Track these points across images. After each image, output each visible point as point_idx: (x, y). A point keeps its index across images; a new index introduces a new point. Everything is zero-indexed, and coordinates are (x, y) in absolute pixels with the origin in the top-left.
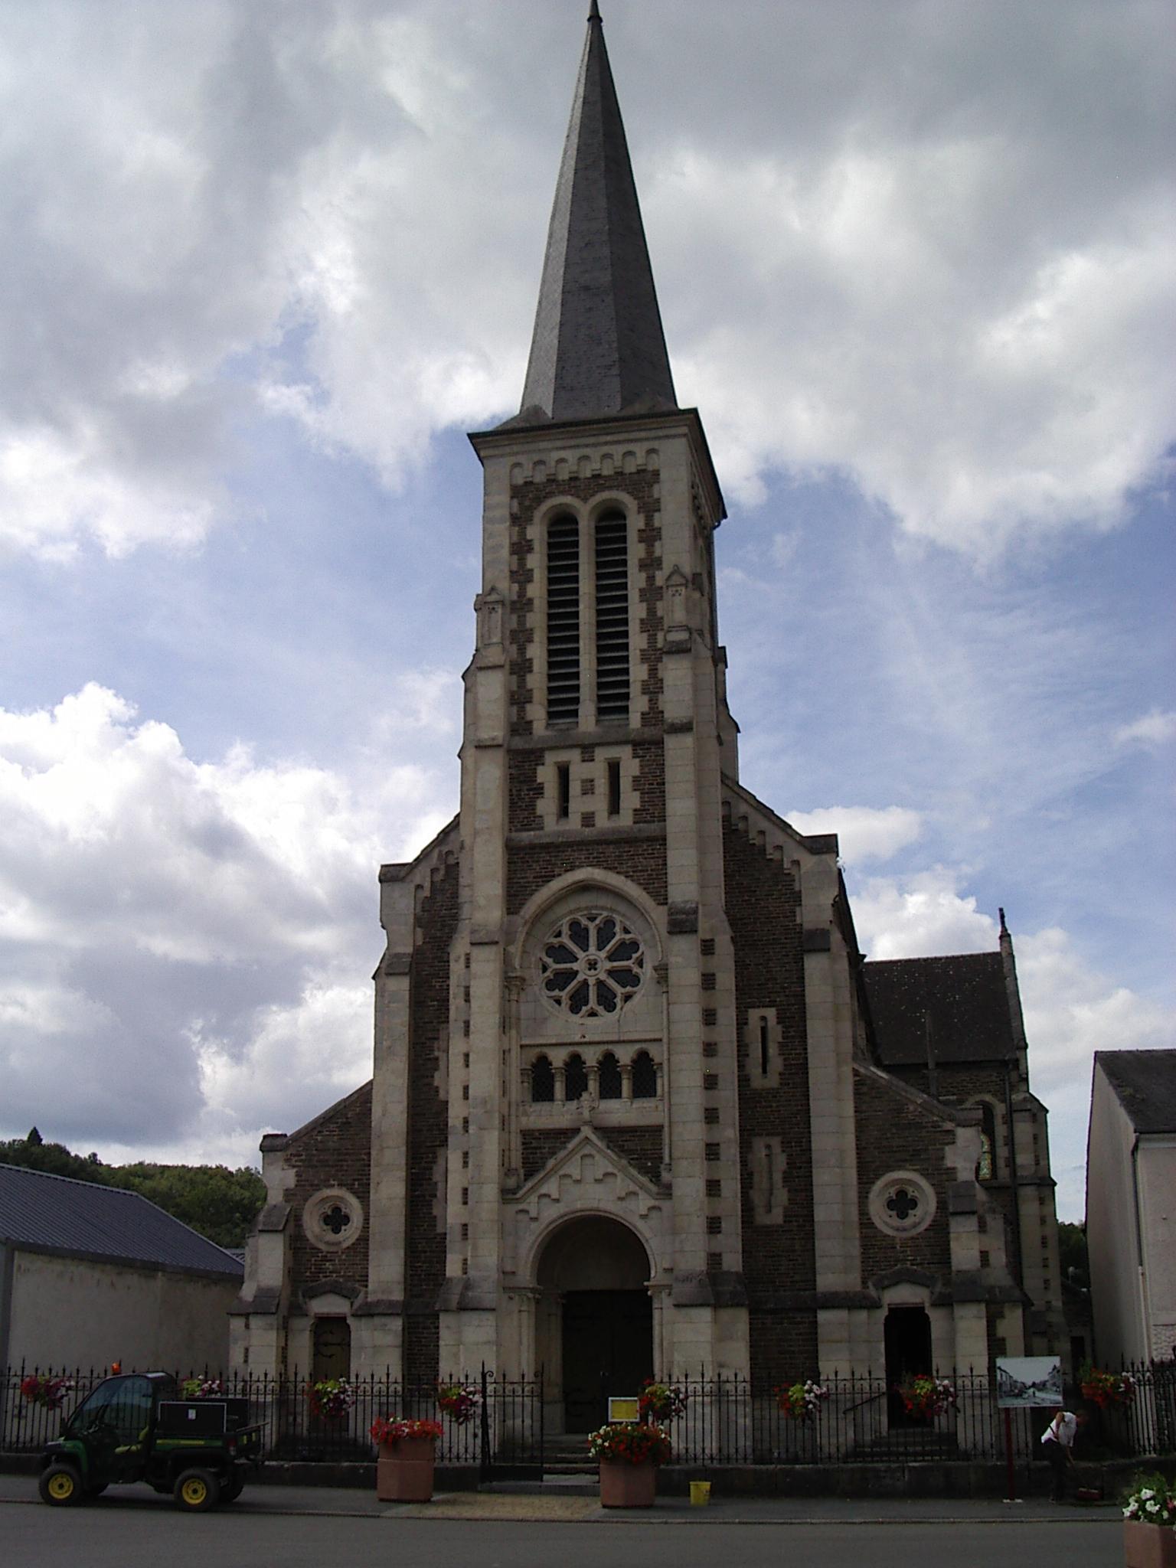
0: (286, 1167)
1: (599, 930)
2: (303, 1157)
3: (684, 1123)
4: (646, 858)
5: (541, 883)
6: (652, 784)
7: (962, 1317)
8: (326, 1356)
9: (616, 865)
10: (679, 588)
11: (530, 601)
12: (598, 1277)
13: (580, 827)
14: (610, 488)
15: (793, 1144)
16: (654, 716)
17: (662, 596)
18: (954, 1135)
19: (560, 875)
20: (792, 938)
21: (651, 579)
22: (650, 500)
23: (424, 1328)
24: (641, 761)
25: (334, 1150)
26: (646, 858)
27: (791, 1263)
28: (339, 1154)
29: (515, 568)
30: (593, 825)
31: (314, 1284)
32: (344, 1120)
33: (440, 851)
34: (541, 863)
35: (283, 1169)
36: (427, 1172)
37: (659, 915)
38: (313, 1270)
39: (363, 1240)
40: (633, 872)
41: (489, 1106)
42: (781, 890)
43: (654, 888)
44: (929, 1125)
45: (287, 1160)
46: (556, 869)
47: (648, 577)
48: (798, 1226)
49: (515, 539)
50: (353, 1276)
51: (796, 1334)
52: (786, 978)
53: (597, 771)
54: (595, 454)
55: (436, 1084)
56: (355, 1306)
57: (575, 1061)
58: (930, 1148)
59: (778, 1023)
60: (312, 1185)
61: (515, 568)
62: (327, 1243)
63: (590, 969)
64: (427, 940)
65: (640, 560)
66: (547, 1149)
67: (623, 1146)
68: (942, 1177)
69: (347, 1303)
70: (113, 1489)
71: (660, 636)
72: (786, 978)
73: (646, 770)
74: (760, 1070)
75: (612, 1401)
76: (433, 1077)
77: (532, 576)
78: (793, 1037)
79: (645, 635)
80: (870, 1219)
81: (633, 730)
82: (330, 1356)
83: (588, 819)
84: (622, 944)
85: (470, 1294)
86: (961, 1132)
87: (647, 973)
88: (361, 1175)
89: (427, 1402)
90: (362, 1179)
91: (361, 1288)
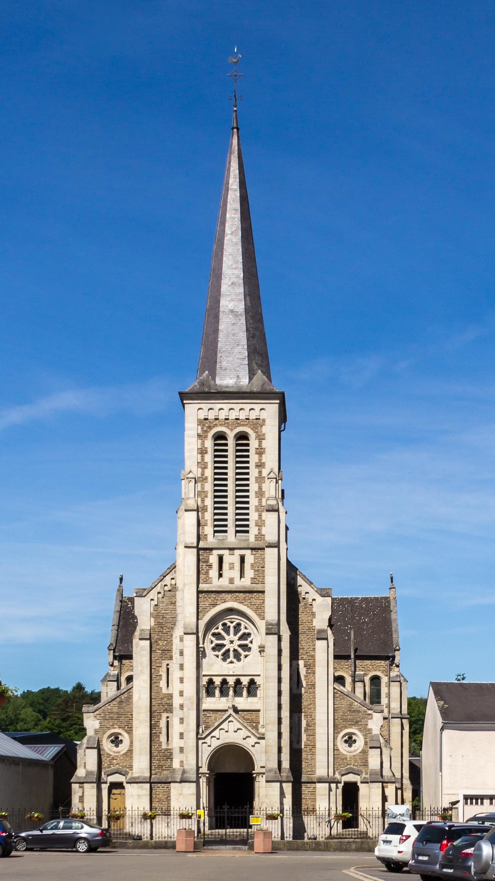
0: (94, 720)
1: (235, 627)
2: (102, 716)
3: (270, 710)
4: (256, 600)
5: (211, 607)
6: (259, 567)
7: (372, 788)
8: (114, 799)
9: (243, 602)
10: (273, 480)
11: (206, 478)
12: (230, 768)
13: (228, 583)
14: (243, 425)
15: (309, 717)
16: (260, 536)
17: (265, 481)
18: (372, 716)
19: (219, 604)
20: (311, 632)
21: (260, 472)
22: (261, 434)
23: (157, 787)
24: (254, 557)
25: (116, 712)
26: (256, 600)
27: (307, 764)
28: (118, 715)
29: (199, 461)
30: (234, 583)
31: (109, 769)
32: (120, 700)
33: (162, 585)
34: (212, 598)
35: (93, 721)
36: (158, 723)
37: (262, 625)
38: (108, 763)
39: (130, 751)
40: (250, 605)
41: (192, 700)
42: (308, 611)
43: (259, 612)
44: (363, 711)
45: (95, 717)
46: (218, 602)
47: (259, 472)
48: (310, 749)
49: (199, 447)
50: (126, 766)
51: (308, 792)
52: (308, 648)
53: (235, 558)
54: (237, 407)
55: (161, 686)
56: (127, 779)
57: (224, 682)
58: (363, 720)
59: (305, 667)
60: (106, 728)
61: (199, 461)
62: (114, 752)
63: (231, 644)
64: (156, 624)
65: (256, 463)
66: (213, 718)
67: (244, 717)
68: (367, 732)
69: (124, 777)
70: (99, 850)
71: (264, 500)
72: (308, 648)
73: (256, 561)
74: (296, 686)
75: (251, 817)
76: (159, 683)
77: (207, 466)
78: (310, 673)
79: (257, 499)
80: (337, 747)
81: (251, 542)
82: (116, 799)
83: (231, 581)
84: (244, 634)
85: (185, 775)
86: (375, 715)
87: (255, 647)
88: (128, 723)
89: (159, 817)
90: (128, 725)
91: (129, 771)
